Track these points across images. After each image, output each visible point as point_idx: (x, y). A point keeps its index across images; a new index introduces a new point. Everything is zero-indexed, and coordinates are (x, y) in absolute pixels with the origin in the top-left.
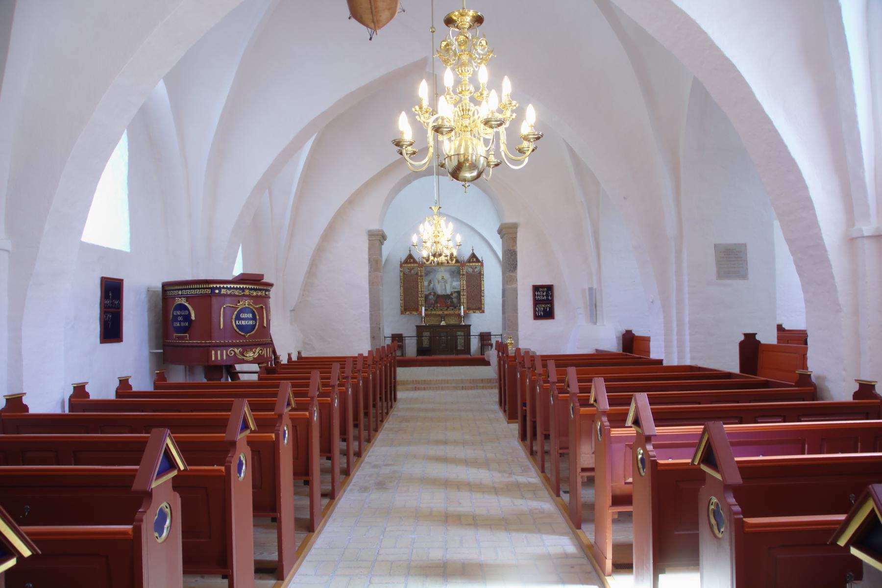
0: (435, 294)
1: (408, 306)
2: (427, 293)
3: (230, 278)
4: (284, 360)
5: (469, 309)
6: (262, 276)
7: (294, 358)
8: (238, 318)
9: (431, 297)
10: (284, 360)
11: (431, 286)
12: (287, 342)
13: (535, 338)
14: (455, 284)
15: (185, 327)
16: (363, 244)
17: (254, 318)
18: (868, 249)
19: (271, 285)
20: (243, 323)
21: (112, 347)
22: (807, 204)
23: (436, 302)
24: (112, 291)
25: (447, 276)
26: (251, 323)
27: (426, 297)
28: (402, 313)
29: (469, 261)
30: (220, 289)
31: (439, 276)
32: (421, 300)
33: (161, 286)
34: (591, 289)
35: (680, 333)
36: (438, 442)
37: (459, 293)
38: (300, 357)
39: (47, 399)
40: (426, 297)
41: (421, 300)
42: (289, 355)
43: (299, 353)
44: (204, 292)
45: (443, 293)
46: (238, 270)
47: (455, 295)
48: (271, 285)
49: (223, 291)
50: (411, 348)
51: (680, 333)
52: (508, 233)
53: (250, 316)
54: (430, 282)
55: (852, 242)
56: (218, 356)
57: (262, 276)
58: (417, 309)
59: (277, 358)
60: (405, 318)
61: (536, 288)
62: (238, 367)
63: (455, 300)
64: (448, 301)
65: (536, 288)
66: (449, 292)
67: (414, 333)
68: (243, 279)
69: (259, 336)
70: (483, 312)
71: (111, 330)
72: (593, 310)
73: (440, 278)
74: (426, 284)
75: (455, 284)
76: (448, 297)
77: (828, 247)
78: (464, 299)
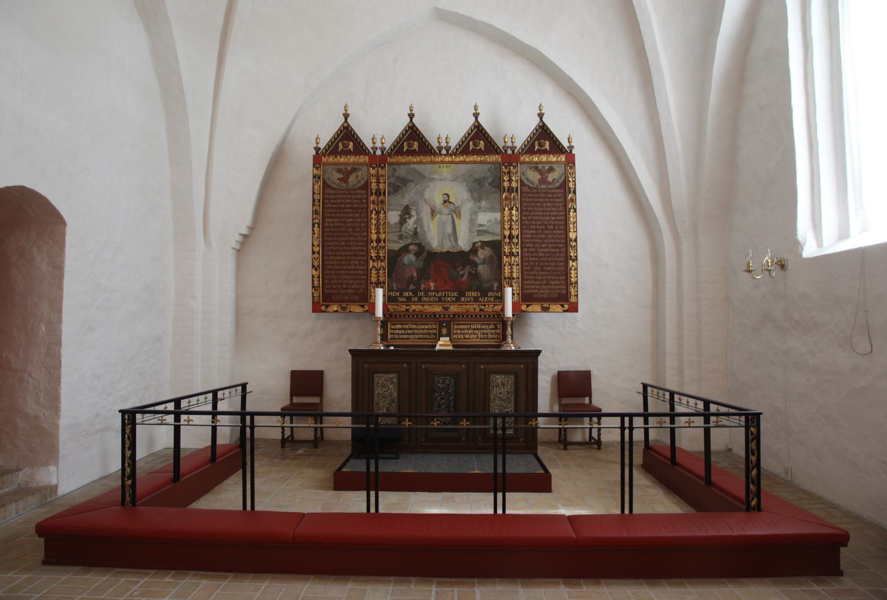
2: (396, 247)
9: (409, 258)
11: (411, 223)
14: (487, 218)
21: (573, 364)
25: (460, 194)
28: (316, 308)
31: (435, 194)
32: (377, 268)
37: (496, 246)
40: (394, 258)
41: (377, 268)
45: (447, 247)
47: (483, 254)
54: (406, 212)
58: (366, 300)
63: (483, 270)
64: (453, 271)
66: (464, 244)
73: (438, 201)
74: (393, 217)
75: (487, 218)
76: (463, 258)
78: (512, 267)
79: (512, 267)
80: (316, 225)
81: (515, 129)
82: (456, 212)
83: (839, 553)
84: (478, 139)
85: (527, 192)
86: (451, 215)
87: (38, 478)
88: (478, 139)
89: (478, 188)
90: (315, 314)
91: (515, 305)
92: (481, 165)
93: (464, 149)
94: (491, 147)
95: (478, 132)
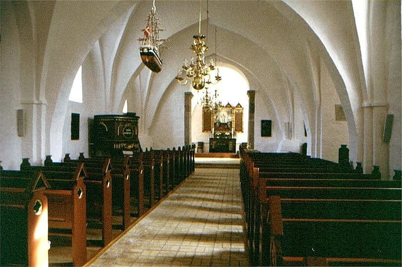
0: (219, 123)
1: (206, 128)
2: (215, 122)
3: (122, 114)
4: (144, 150)
5: (236, 130)
6: (135, 114)
7: (149, 150)
8: (125, 131)
9: (217, 124)
10: (144, 150)
11: (218, 118)
12: (146, 142)
13: (262, 145)
14: (230, 118)
15: (127, 129)
16: (182, 98)
17: (131, 131)
18: (366, 111)
19: (139, 117)
20: (127, 133)
21: (75, 141)
22: (346, 93)
23: (220, 126)
24: (75, 118)
25: (226, 114)
26: (130, 133)
27: (215, 124)
28: (203, 132)
29: (237, 107)
30: (118, 119)
31: (221, 114)
32: (212, 125)
33: (93, 117)
34: (288, 123)
35: (318, 144)
36: (206, 187)
37: (231, 122)
38: (151, 150)
39: (57, 158)
40: (215, 124)
41: (212, 125)
42: (147, 149)
43: (151, 148)
44: (111, 120)
45: (223, 122)
46: (125, 111)
47: (229, 123)
48: (139, 117)
49: (119, 120)
50: (207, 147)
51: (318, 144)
52: (251, 94)
53: (130, 130)
54: (217, 117)
55: (361, 109)
56: (116, 146)
57: (135, 114)
58: (210, 130)
59: (141, 149)
60: (205, 133)
61: (263, 122)
62: (124, 152)
63: (229, 126)
64: (225, 126)
65: (263, 122)
66: (226, 122)
67: (208, 142)
68: (128, 114)
69: (135, 140)
70: (243, 132)
71: (75, 135)
72: (290, 132)
73: (222, 115)
74: (215, 117)
75: (230, 118)
76: (226, 124)
77: (353, 110)
78: (233, 126)
79: (233, 126)
80: (366, 111)
81: (234, 104)
82: (225, 117)
83: (54, 163)
84: (229, 105)
85: (237, 114)
86: (224, 117)
87: (34, 162)
88: (229, 105)
89: (228, 113)
90: (273, 133)
91: (234, 132)
92: (228, 109)
93: (226, 107)
94: (231, 106)
95: (229, 104)
